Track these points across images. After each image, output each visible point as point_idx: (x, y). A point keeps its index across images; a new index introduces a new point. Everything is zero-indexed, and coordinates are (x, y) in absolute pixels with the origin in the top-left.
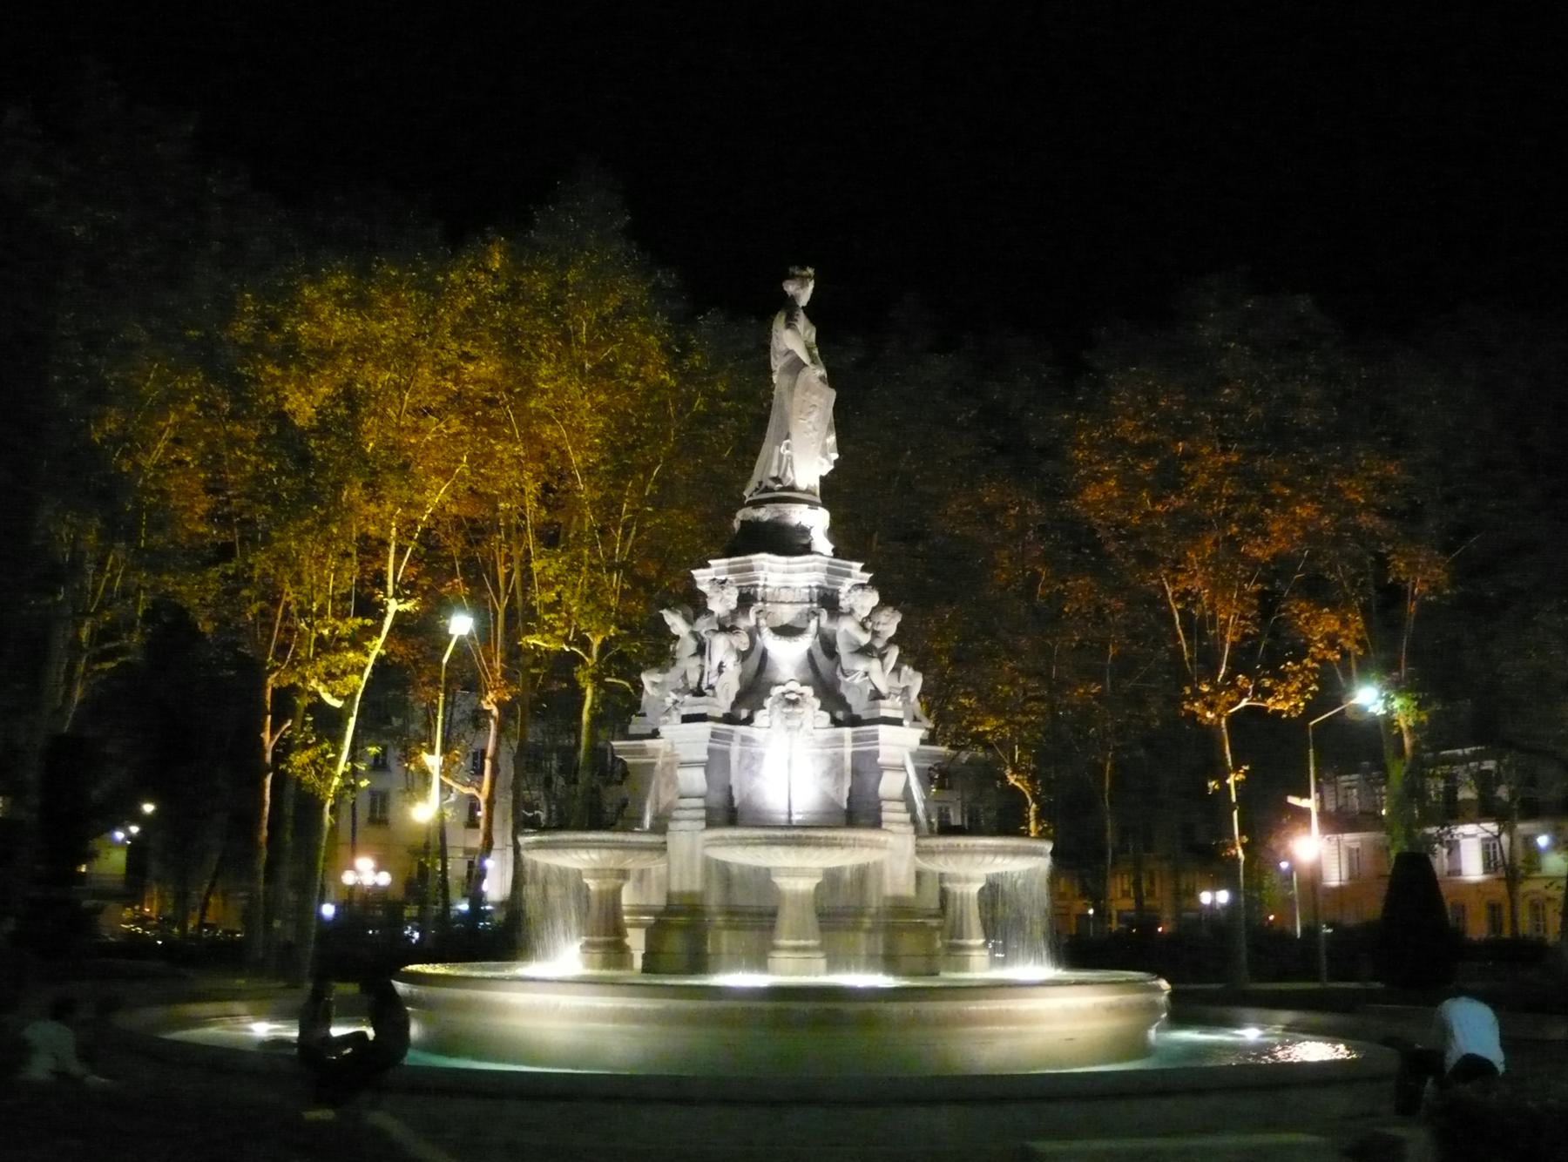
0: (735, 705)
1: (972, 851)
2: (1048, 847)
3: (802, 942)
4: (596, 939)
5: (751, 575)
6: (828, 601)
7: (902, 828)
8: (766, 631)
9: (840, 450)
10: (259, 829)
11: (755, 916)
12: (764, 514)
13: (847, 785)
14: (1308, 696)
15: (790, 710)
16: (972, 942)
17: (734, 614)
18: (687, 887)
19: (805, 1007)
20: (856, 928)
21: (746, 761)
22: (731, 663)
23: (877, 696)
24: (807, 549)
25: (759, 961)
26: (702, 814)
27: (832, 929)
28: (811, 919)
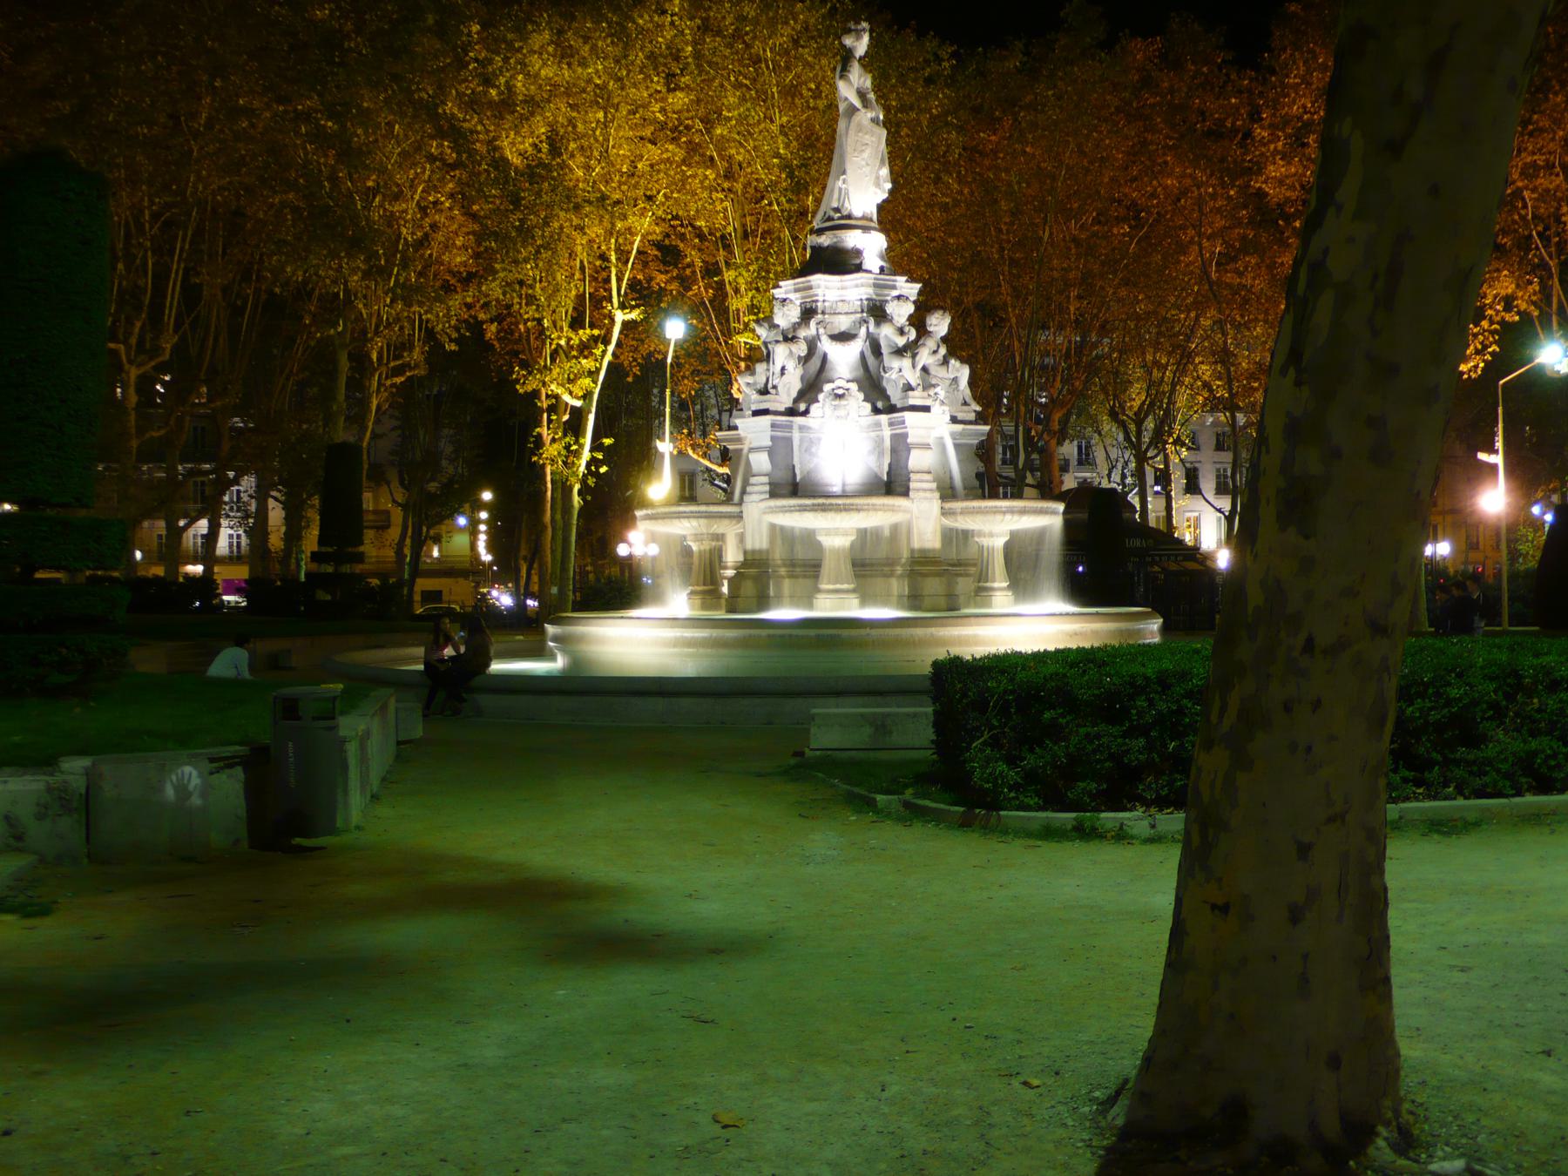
0: (796, 401)
1: (996, 511)
2: (1061, 507)
3: (838, 586)
5: (811, 292)
6: (877, 312)
7: (928, 495)
8: (824, 339)
10: (543, 511)
11: (806, 565)
12: (825, 240)
13: (887, 460)
14: (1488, 357)
15: (837, 402)
16: (996, 585)
17: (796, 327)
18: (757, 546)
20: (891, 575)
21: (805, 445)
22: (791, 365)
23: (908, 388)
24: (858, 268)
26: (767, 488)
27: (864, 576)
28: (846, 569)
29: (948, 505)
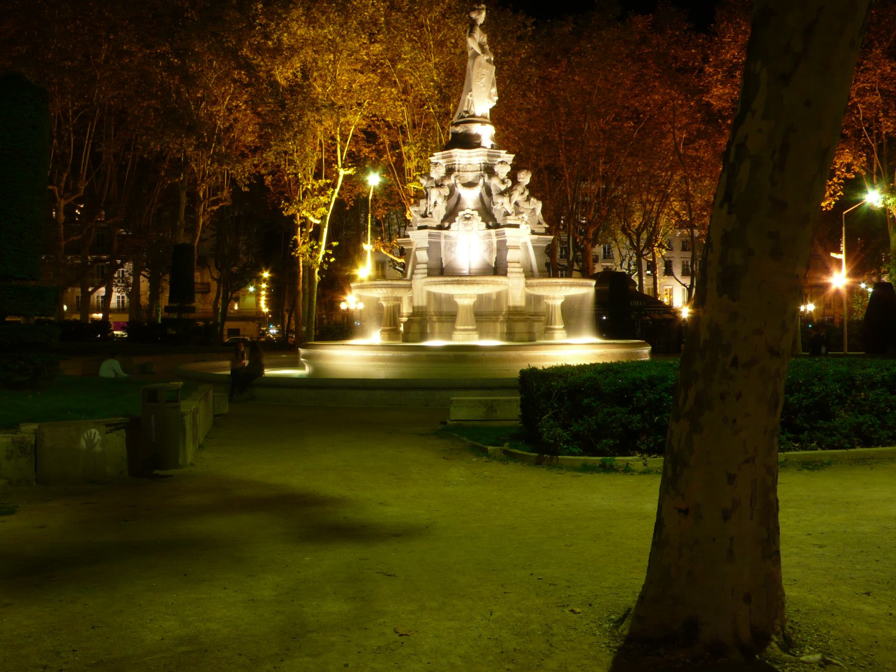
0: (443, 221)
1: (557, 285)
2: (594, 283)
3: (466, 327)
4: (388, 328)
6: (489, 170)
7: (518, 275)
8: (459, 186)
9: (499, 96)
10: (298, 284)
11: (448, 315)
12: (460, 129)
14: (837, 198)
17: (443, 179)
18: (420, 304)
19: (451, 353)
20: (495, 321)
21: (448, 247)
23: (507, 214)
24: (479, 146)
25: (449, 336)
26: (426, 271)
27: (482, 322)
29: (529, 281)
